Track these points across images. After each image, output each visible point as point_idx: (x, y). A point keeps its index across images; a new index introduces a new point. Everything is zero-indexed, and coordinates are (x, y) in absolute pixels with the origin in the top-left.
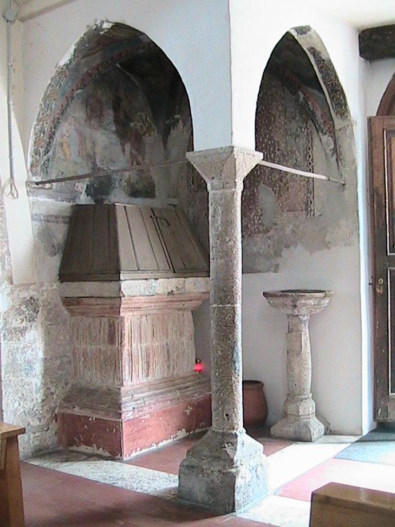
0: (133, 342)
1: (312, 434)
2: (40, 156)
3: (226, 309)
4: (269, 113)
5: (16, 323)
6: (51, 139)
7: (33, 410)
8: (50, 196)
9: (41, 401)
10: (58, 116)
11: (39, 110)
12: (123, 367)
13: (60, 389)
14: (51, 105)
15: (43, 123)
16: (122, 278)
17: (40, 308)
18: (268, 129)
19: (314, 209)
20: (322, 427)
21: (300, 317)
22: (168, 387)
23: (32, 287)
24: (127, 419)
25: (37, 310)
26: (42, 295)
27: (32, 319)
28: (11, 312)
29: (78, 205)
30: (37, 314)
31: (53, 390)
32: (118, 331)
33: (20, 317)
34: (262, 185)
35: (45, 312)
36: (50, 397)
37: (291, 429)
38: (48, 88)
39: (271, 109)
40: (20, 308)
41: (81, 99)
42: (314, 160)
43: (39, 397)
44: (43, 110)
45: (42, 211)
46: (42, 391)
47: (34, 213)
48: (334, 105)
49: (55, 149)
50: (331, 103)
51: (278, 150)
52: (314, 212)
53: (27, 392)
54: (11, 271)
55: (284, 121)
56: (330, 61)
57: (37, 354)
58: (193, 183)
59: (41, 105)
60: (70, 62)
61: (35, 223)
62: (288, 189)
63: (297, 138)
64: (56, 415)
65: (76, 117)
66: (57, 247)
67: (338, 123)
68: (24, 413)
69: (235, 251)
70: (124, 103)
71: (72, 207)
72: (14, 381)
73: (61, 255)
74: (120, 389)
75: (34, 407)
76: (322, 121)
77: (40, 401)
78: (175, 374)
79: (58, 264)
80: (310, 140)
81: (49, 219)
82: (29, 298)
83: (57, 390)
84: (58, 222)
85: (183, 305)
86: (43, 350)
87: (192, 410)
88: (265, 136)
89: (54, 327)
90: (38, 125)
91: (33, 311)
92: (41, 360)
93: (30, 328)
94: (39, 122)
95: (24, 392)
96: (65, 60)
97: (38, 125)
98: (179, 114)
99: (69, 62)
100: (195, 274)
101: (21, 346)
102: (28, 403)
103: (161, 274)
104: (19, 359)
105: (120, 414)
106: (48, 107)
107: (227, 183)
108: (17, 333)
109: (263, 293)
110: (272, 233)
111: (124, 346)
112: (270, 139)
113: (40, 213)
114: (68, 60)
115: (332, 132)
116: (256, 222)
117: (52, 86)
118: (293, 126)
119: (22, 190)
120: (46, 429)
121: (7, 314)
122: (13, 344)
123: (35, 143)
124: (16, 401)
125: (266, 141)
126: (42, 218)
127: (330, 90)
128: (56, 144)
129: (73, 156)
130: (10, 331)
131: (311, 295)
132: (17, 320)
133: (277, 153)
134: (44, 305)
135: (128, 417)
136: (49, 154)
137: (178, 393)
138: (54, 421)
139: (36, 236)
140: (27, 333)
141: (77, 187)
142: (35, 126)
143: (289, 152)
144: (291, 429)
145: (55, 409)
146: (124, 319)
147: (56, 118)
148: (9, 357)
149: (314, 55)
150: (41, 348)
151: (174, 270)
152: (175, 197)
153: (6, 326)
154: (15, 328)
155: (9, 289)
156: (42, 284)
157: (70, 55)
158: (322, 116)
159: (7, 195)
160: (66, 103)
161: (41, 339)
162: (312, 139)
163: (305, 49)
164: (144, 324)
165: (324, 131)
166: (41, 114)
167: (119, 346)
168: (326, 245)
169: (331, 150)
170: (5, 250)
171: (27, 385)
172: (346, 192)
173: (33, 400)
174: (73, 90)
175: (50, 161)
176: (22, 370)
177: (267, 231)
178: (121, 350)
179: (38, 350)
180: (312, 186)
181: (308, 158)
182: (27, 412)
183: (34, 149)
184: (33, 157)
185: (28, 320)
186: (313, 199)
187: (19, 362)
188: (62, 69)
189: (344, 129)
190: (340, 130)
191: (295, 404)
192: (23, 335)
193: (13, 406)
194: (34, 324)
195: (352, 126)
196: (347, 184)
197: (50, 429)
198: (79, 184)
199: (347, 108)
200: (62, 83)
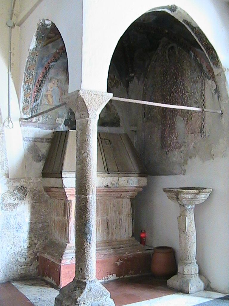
1: (189, 289)
2: (29, 103)
3: (81, 198)
4: (182, 68)
6: (38, 93)
7: (21, 252)
8: (36, 126)
9: (27, 247)
10: (41, 79)
11: (24, 76)
12: (70, 231)
13: (41, 241)
14: (31, 73)
15: (28, 84)
16: (63, 176)
18: (182, 79)
19: (205, 132)
20: (202, 285)
21: (185, 206)
22: (106, 246)
24: (65, 264)
25: (26, 194)
26: (30, 185)
28: (7, 194)
29: (57, 132)
30: (26, 196)
31: (36, 241)
32: (68, 209)
33: (13, 197)
34: (178, 116)
35: (32, 195)
36: (33, 245)
37: (178, 284)
38: (27, 63)
39: (184, 66)
41: (63, 68)
42: (205, 98)
43: (26, 245)
44: (27, 76)
46: (27, 241)
47: (25, 137)
48: (211, 58)
49: (42, 98)
50: (209, 56)
51: (187, 92)
52: (205, 133)
53: (17, 241)
54: (8, 171)
55: (190, 73)
56: (199, 28)
57: (25, 219)
58: (145, 117)
60: (36, 46)
62: (192, 118)
63: (197, 84)
64: (38, 257)
65: (58, 79)
66: (41, 157)
67: (216, 71)
68: (14, 254)
69: (88, 160)
71: (53, 133)
72: (8, 234)
73: (45, 161)
74: (66, 244)
75: (21, 251)
76: (207, 70)
77: (26, 247)
78: (114, 238)
79: (42, 167)
80: (203, 85)
81: (36, 140)
82: (20, 186)
83: (38, 242)
84: (42, 142)
85: (121, 195)
87: (122, 263)
88: (180, 83)
89: (38, 204)
90: (25, 85)
92: (28, 223)
93: (20, 204)
94: (25, 83)
95: (15, 241)
96: (33, 45)
97: (25, 85)
98: (132, 73)
99: (36, 47)
101: (14, 214)
102: (17, 248)
104: (12, 222)
105: (61, 260)
107: (82, 115)
108: (11, 206)
109: (163, 189)
110: (182, 149)
111: (71, 218)
112: (183, 85)
113: (29, 136)
114: (35, 45)
115: (213, 77)
116: (175, 141)
118: (195, 75)
119: (17, 123)
120: (30, 264)
121: (4, 195)
122: (8, 212)
123: (24, 95)
124: (8, 246)
125: (180, 87)
126: (31, 139)
127: (205, 48)
128: (42, 96)
130: (5, 205)
131: (187, 191)
132: (11, 199)
133: (186, 94)
134: (31, 191)
135: (66, 263)
136: (38, 101)
137: (112, 250)
138: (36, 261)
139: (25, 150)
141: (58, 121)
142: (24, 85)
143: (193, 93)
144: (178, 284)
145: (37, 253)
146: (72, 201)
147: (39, 80)
148: (4, 220)
149: (188, 25)
150: (27, 216)
151: (108, 172)
152: (136, 126)
153: (3, 202)
154: (9, 204)
155: (6, 181)
157: (35, 43)
158: (207, 67)
159: (6, 126)
160: (45, 71)
162: (204, 83)
163: (181, 22)
165: (209, 77)
166: (26, 79)
167: (68, 218)
168: (212, 156)
169: (214, 90)
170: (4, 158)
171: (17, 237)
172: (223, 119)
173: (21, 247)
174: (49, 63)
175: (39, 106)
176: (14, 228)
177: (180, 147)
178: (69, 221)
180: (204, 116)
181: (202, 96)
182: (16, 253)
184: (24, 104)
185: (19, 200)
186: (205, 125)
188: (33, 51)
189: (219, 75)
190: (217, 75)
191: (182, 266)
192: (15, 208)
193: (7, 248)
194: (23, 202)
195: (224, 72)
196: (224, 114)
197: (33, 265)
198: (59, 119)
199: (218, 59)
200: (36, 59)
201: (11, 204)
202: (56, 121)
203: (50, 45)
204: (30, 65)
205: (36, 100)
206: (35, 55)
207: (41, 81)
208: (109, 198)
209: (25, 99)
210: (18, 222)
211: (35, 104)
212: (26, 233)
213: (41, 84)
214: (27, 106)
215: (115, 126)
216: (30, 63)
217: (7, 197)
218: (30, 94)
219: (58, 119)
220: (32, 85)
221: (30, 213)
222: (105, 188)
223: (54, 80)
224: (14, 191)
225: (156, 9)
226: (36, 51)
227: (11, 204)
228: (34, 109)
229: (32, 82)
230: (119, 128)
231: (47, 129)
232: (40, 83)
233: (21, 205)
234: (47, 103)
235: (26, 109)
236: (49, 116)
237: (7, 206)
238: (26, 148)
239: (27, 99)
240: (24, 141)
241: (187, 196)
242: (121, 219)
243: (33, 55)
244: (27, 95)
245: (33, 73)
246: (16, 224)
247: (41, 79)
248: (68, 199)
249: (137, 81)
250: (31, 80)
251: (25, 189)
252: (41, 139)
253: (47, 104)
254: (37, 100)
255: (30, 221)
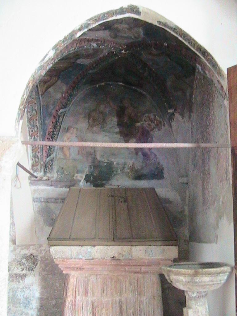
0: (77, 295)
5: (18, 270)
11: (28, 129)
15: (35, 137)
17: (39, 262)
23: (31, 247)
25: (36, 263)
27: (31, 269)
33: (21, 267)
35: (43, 265)
40: (21, 261)
45: (44, 195)
54: (15, 237)
59: (28, 126)
61: (36, 203)
70: (129, 110)
84: (57, 202)
86: (39, 291)
89: (51, 276)
91: (32, 263)
97: (31, 138)
98: (170, 108)
100: (144, 243)
101: (21, 287)
103: (96, 242)
104: (19, 295)
106: (34, 126)
108: (18, 277)
113: (40, 197)
117: (30, 112)
122: (14, 284)
123: (32, 150)
129: (73, 155)
132: (18, 269)
134: (41, 260)
140: (26, 279)
141: (77, 177)
154: (16, 274)
155: (13, 247)
156: (41, 246)
161: (37, 283)
164: (93, 282)
166: (31, 131)
174: (57, 111)
179: (35, 291)
183: (33, 155)
184: (32, 160)
185: (28, 270)
187: (19, 297)
201: (18, 275)
202: (75, 177)
203: (51, 90)
204: (31, 115)
205: (49, 154)
206: (33, 104)
207: (52, 133)
208: (123, 274)
209: (34, 154)
210: (26, 296)
211: (48, 158)
212: (35, 310)
213: (53, 136)
214: (36, 162)
215: (156, 178)
216: (30, 113)
217: (14, 266)
218: (38, 149)
219: (76, 175)
220: (39, 138)
221: (40, 287)
222: (112, 260)
223: (72, 129)
224: (22, 260)
225: (109, 17)
226: (32, 100)
227: (18, 275)
228: (47, 165)
229: (38, 135)
230: (163, 180)
231: (62, 188)
232: (51, 134)
233: (30, 276)
234: (62, 157)
235: (36, 166)
236: (65, 172)
237: (13, 277)
238: (37, 210)
239: (36, 154)
240: (34, 202)
241: (179, 278)
242: (141, 302)
243: (31, 104)
244: (36, 149)
245: (38, 125)
246: (24, 298)
247: (51, 130)
248: (64, 272)
249: (180, 118)
250: (36, 133)
251: (36, 257)
252: (56, 199)
253: (63, 158)
254: (50, 154)
255: (40, 295)
